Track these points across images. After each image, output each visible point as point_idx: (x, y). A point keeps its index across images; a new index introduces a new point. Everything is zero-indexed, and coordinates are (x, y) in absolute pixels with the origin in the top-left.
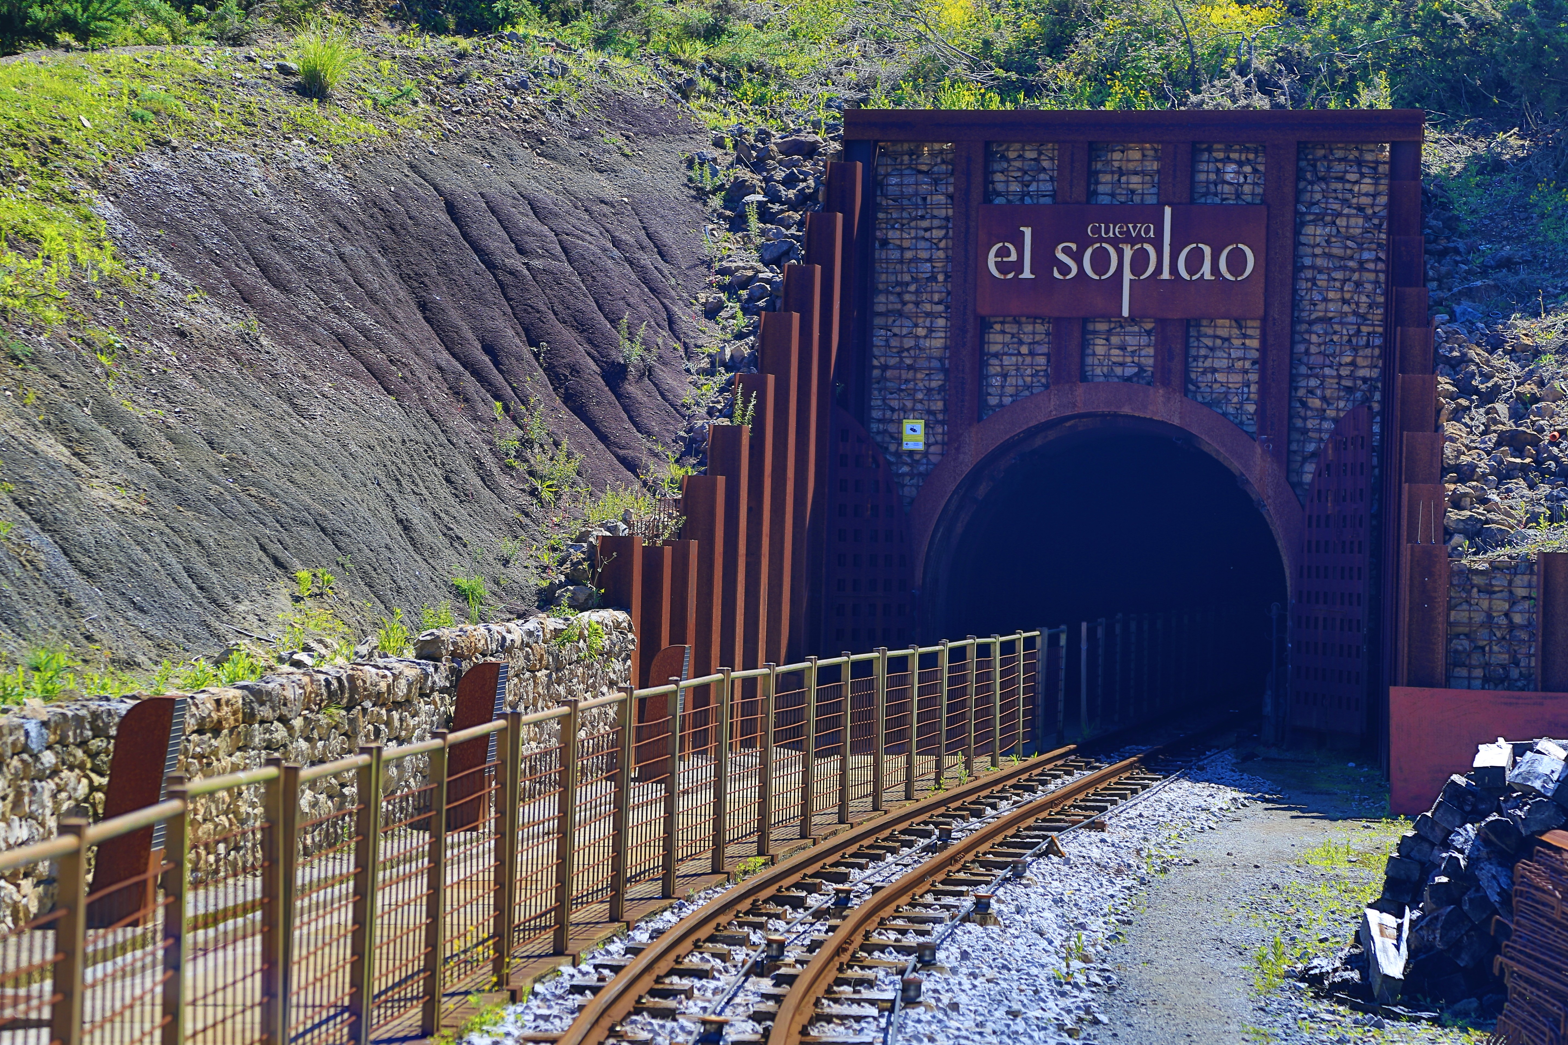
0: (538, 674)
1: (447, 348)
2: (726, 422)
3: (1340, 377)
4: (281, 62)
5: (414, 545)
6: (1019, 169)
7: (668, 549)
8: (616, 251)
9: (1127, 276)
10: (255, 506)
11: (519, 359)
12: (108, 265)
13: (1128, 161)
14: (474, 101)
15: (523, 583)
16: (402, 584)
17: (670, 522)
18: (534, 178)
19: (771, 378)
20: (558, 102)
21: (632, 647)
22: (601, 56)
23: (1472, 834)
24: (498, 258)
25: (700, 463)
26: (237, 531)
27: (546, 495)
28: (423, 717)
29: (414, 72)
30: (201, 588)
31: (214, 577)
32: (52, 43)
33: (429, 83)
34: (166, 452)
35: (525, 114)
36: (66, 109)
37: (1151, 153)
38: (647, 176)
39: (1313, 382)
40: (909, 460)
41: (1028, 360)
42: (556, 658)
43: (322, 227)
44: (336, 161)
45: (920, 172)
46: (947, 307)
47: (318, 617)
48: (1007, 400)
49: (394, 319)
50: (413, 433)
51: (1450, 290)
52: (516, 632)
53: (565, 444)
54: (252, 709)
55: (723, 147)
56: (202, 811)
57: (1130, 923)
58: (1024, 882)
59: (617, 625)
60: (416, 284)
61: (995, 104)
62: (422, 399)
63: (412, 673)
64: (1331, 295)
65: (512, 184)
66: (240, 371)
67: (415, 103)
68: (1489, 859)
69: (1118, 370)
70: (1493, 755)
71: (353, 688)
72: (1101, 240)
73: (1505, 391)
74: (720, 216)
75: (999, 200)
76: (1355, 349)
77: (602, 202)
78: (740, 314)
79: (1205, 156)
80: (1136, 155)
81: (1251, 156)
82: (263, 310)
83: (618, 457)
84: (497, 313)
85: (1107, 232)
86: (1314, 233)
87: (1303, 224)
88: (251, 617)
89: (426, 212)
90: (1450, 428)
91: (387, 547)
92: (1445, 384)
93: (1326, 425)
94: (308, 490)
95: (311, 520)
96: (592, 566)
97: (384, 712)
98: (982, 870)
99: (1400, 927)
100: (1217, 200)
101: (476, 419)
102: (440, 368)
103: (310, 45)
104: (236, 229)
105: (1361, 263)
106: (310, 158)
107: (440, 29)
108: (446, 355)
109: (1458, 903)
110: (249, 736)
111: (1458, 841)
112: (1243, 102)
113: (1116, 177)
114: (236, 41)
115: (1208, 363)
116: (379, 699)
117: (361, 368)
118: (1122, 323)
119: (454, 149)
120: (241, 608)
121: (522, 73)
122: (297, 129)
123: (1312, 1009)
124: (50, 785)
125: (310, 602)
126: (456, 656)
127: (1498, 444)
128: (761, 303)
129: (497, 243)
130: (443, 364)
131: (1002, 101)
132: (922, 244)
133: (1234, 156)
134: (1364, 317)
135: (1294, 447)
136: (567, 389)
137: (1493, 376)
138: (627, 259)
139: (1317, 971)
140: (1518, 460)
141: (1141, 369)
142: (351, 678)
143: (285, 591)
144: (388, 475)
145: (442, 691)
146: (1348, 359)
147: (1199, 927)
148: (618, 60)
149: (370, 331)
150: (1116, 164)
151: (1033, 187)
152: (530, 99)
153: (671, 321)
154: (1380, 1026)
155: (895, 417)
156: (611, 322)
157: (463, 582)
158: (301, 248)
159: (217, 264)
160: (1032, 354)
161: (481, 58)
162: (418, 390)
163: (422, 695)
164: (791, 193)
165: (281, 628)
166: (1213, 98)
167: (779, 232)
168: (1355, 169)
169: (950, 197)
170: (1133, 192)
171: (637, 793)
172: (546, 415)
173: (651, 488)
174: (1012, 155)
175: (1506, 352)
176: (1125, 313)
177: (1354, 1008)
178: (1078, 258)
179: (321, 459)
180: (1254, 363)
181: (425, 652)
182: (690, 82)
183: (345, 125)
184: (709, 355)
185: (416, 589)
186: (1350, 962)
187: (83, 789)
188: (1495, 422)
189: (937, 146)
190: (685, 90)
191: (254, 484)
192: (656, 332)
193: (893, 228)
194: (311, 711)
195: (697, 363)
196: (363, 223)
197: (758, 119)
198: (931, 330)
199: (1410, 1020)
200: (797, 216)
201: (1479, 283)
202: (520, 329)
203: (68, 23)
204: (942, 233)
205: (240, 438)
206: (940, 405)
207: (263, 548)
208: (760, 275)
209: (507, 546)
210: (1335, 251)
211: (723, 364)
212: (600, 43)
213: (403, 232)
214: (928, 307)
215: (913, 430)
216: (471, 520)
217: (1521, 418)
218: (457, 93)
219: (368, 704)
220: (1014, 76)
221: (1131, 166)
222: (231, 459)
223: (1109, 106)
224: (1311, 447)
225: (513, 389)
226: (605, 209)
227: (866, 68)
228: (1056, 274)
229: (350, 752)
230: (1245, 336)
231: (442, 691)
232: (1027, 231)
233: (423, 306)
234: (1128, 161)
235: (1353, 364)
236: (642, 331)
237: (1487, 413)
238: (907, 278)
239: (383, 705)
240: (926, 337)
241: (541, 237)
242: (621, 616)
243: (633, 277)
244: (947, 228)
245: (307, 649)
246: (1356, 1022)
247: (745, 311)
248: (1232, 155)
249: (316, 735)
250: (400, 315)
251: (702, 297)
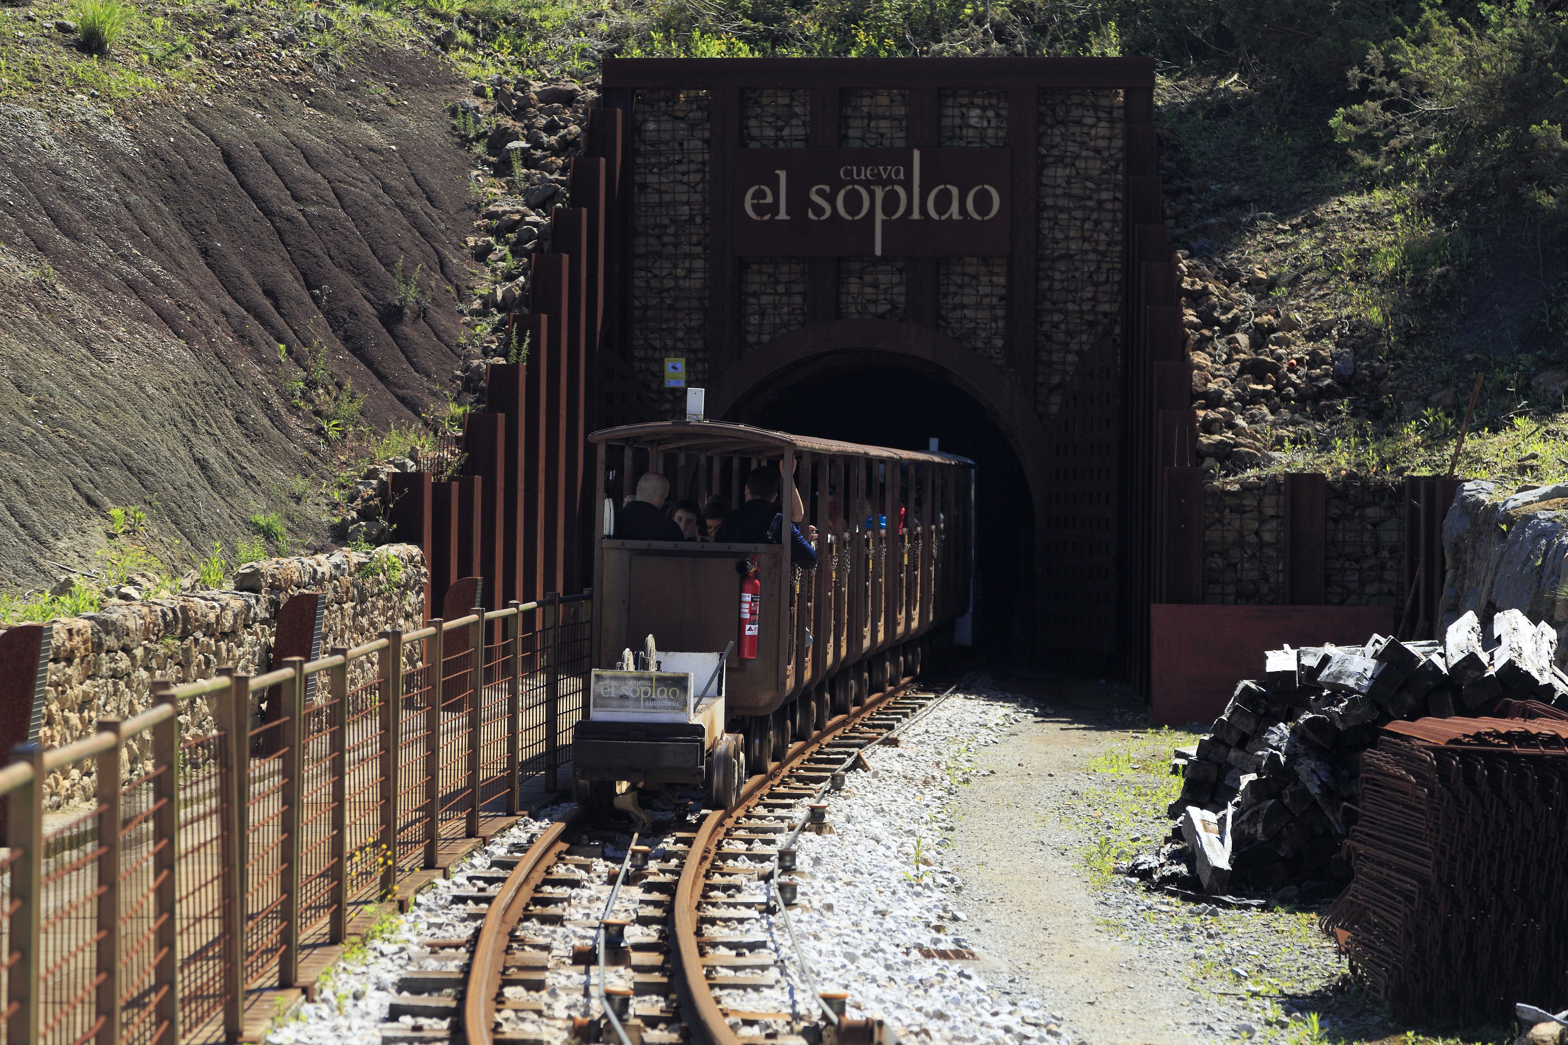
0: (345, 606)
1: (230, 293)
2: (502, 361)
3: (1082, 312)
4: (60, 21)
5: (211, 484)
6: (773, 115)
7: (455, 485)
8: (386, 197)
9: (879, 217)
10: (65, 447)
11: (299, 303)
13: (877, 106)
14: (244, 55)
15: (316, 519)
16: (205, 521)
17: (451, 456)
18: (305, 127)
19: (544, 318)
20: (324, 55)
21: (424, 580)
23: (1287, 732)
24: (275, 205)
25: (478, 401)
26: (51, 471)
27: (333, 434)
28: (247, 648)
29: (185, 29)
30: (23, 526)
31: (34, 515)
33: (201, 38)
35: (294, 66)
37: (899, 98)
38: (412, 125)
39: (1057, 317)
40: (670, 397)
41: (785, 299)
42: (361, 591)
43: (108, 177)
44: (118, 114)
45: (677, 118)
46: (705, 249)
47: (133, 556)
48: (765, 338)
49: (179, 265)
50: (203, 375)
51: (1186, 227)
52: (325, 564)
53: (349, 385)
54: (100, 638)
55: (484, 96)
56: (58, 738)
57: (952, 829)
58: (843, 794)
59: (411, 559)
60: (197, 232)
62: (210, 342)
63: (237, 604)
64: (1072, 234)
65: (285, 134)
66: (39, 317)
67: (188, 58)
68: (1307, 755)
69: (872, 308)
70: (1281, 660)
71: (186, 619)
72: (854, 182)
73: (1244, 322)
74: (485, 162)
75: (753, 145)
76: (1096, 285)
77: (371, 150)
78: (509, 257)
79: (951, 101)
80: (884, 100)
81: (994, 101)
82: (57, 258)
83: (397, 396)
84: (276, 259)
85: (859, 174)
86: (1057, 174)
87: (1044, 166)
88: (71, 554)
89: (205, 162)
90: (1199, 358)
91: (189, 486)
92: (1190, 315)
93: (1071, 358)
94: (112, 431)
95: (118, 461)
96: (384, 502)
97: (212, 642)
98: (800, 785)
99: (1222, 822)
100: (963, 143)
101: (260, 362)
102: (225, 313)
104: (28, 180)
105: (1100, 202)
108: (229, 299)
109: (1279, 796)
110: (97, 664)
111: (1273, 739)
112: (981, 50)
113: (866, 122)
115: (957, 300)
116: (209, 630)
117: (152, 313)
118: (876, 261)
119: (229, 100)
120: (61, 545)
121: (289, 28)
122: (79, 84)
123: (1148, 902)
125: (123, 539)
127: (1241, 372)
128: (529, 246)
130: (227, 308)
131: (752, 50)
132: (679, 188)
133: (978, 101)
134: (1103, 254)
135: (1040, 379)
136: (346, 331)
137: (1232, 308)
138: (397, 205)
139: (1145, 866)
140: (1260, 387)
141: (894, 307)
142: (184, 609)
143: (99, 528)
144: (183, 416)
145: (264, 621)
146: (1090, 295)
147: (1017, 831)
148: (380, 14)
149: (158, 277)
150: (866, 109)
151: (786, 132)
152: (298, 52)
153: (443, 265)
154: (1214, 914)
155: (657, 355)
156: (385, 265)
158: (89, 198)
159: (11, 215)
160: (788, 293)
161: (247, 13)
162: (206, 333)
163: (247, 626)
164: (553, 139)
165: (100, 564)
166: (952, 46)
167: (543, 177)
168: (1091, 113)
169: (707, 142)
170: (882, 136)
171: (448, 721)
172: (327, 355)
173: (432, 426)
174: (765, 101)
175: (1242, 285)
176: (878, 252)
177: (1186, 899)
178: (831, 199)
179: (122, 400)
180: (1001, 298)
181: (246, 584)
182: (450, 35)
183: (126, 80)
184: (481, 297)
185: (218, 527)
186: (1175, 857)
188: (1238, 351)
189: (692, 93)
190: (445, 42)
191: (63, 425)
192: (429, 275)
193: (651, 172)
194: (151, 641)
195: (477, 299)
196: (144, 173)
197: (515, 70)
198: (690, 271)
199: (1240, 907)
200: (560, 162)
201: (1213, 221)
202: (298, 274)
204: (699, 177)
205: (45, 382)
206: (699, 344)
207: (76, 487)
208: (527, 219)
209: (299, 484)
210: (1075, 192)
211: (496, 305)
213: (184, 181)
214: (686, 249)
215: (675, 368)
216: (263, 459)
217: (1260, 347)
218: (227, 47)
219: (199, 634)
220: (761, 26)
221: (880, 111)
222: (39, 401)
223: (853, 54)
224: (1056, 379)
225: (295, 332)
226: (375, 156)
227: (617, 20)
228: (811, 216)
229: (184, 681)
230: (992, 273)
231: (264, 621)
232: (782, 175)
233: (205, 253)
234: (877, 106)
235: (1094, 299)
236: (416, 274)
237: (1229, 342)
238: (666, 221)
239: (212, 636)
240: (685, 277)
241: (314, 184)
242: (415, 550)
243: (405, 222)
244: (703, 171)
245: (132, 582)
246: (1191, 912)
247: (514, 253)
248: (976, 101)
249: (154, 665)
250: (184, 261)
251: (471, 241)
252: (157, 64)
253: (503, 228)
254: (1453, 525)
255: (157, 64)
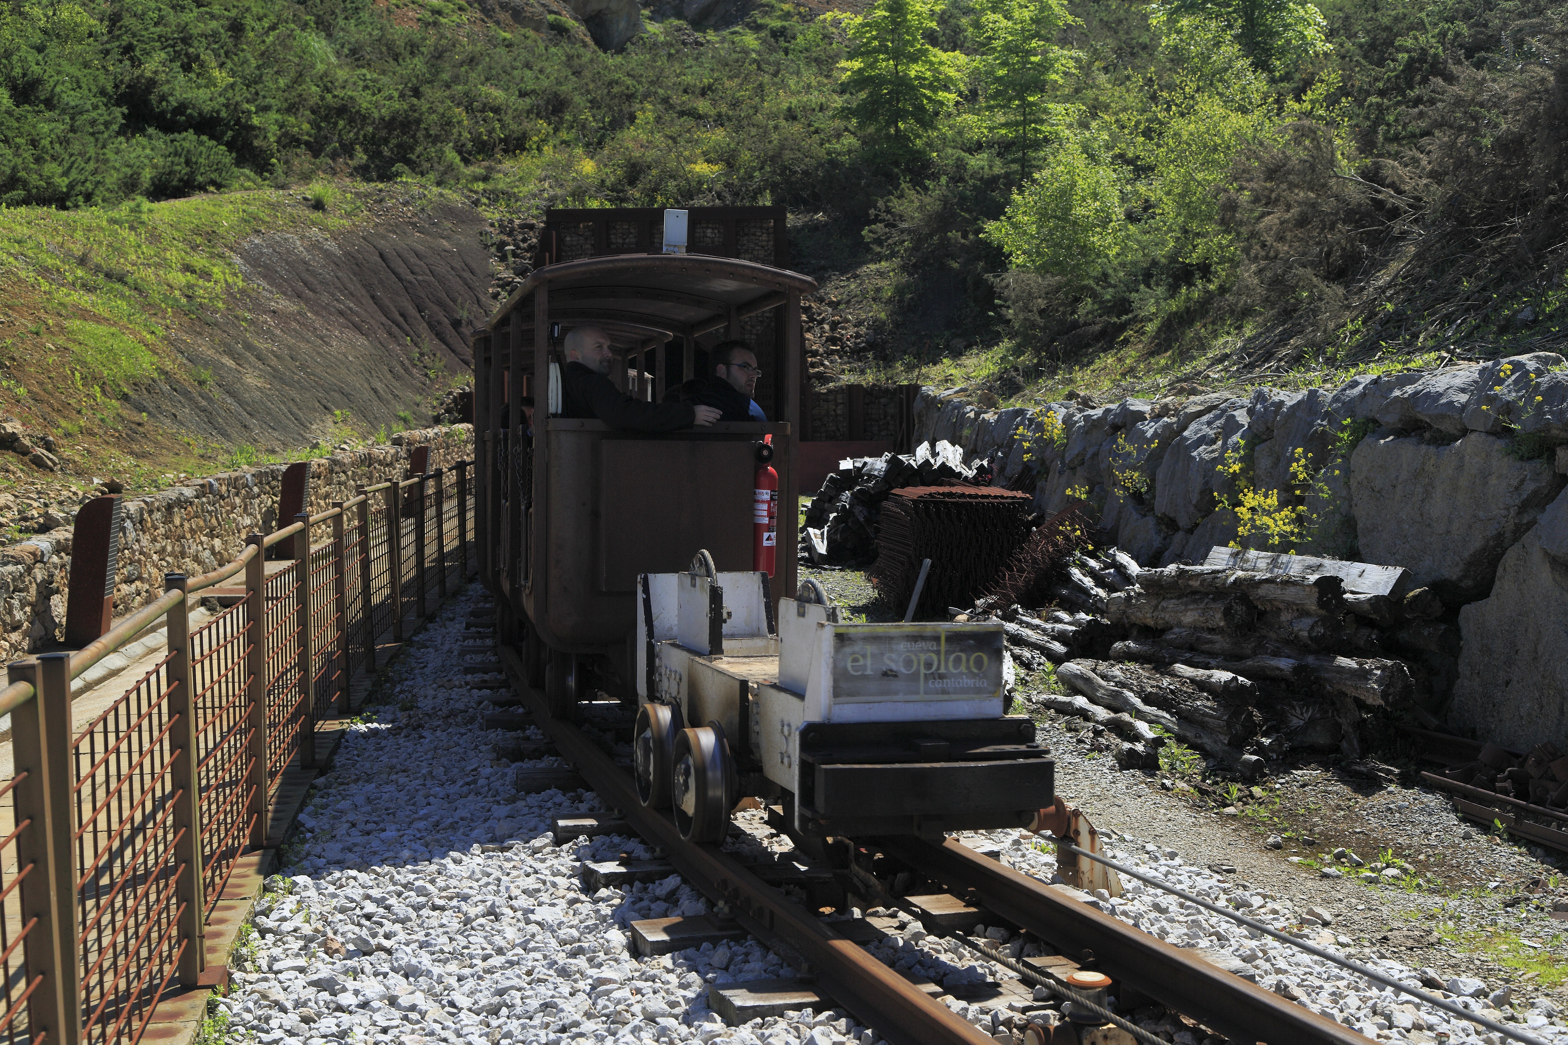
12: (241, 284)
22: (439, 190)
24: (403, 276)
26: (308, 395)
32: (206, 191)
34: (274, 362)
36: (217, 219)
47: (347, 430)
52: (431, 432)
61: (608, 205)
63: (392, 451)
70: (846, 464)
82: (307, 301)
103: (317, 188)
106: (320, 236)
107: (369, 180)
114: (283, 187)
116: (381, 463)
119: (381, 230)
124: (257, 501)
126: (408, 444)
129: (402, 270)
153: (478, 301)
157: (402, 414)
172: (429, 342)
182: (478, 200)
187: (269, 503)
190: (476, 203)
203: (213, 183)
209: (418, 398)
212: (439, 184)
227: (552, 193)
233: (373, 297)
236: (467, 305)
252: (348, 215)
253: (505, 284)
254: (918, 405)
255: (348, 215)
